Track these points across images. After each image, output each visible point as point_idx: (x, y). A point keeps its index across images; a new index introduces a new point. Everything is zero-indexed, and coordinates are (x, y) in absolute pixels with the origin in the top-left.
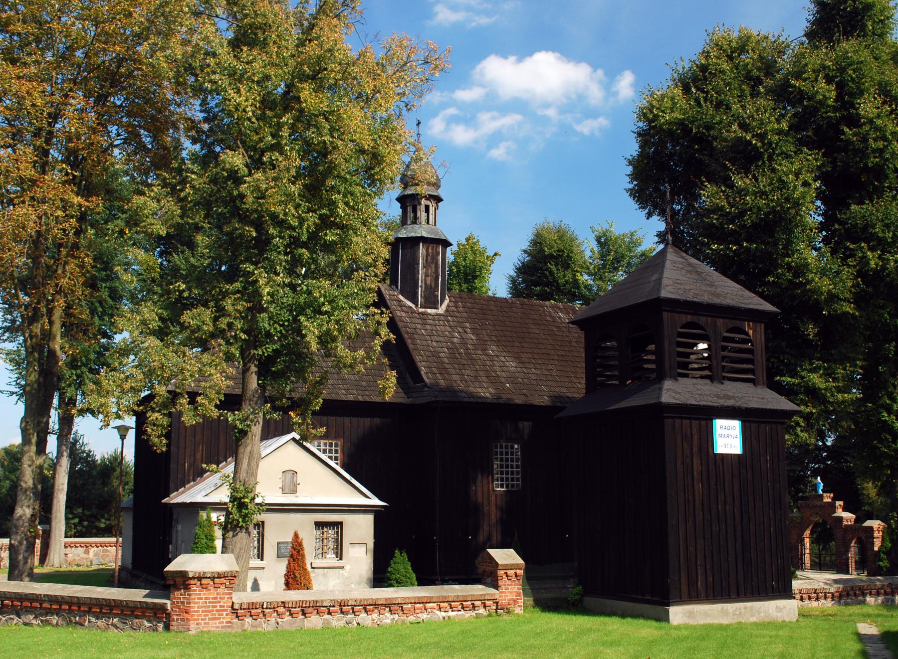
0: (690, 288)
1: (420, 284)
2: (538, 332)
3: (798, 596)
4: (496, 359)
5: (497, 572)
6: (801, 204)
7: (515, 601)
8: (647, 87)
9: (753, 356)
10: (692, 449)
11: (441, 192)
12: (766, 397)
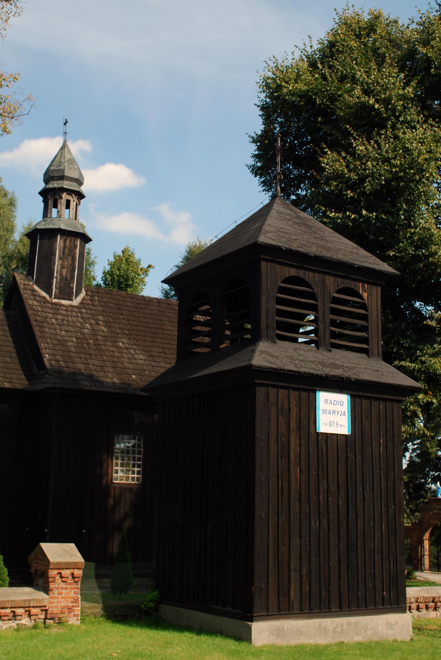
0: (296, 238)
1: (55, 275)
2: (171, 328)
3: (414, 606)
4: (125, 351)
5: (47, 573)
6: (425, 170)
7: (70, 609)
8: (272, 58)
9: (368, 322)
10: (289, 426)
11: (84, 189)
12: (381, 370)
